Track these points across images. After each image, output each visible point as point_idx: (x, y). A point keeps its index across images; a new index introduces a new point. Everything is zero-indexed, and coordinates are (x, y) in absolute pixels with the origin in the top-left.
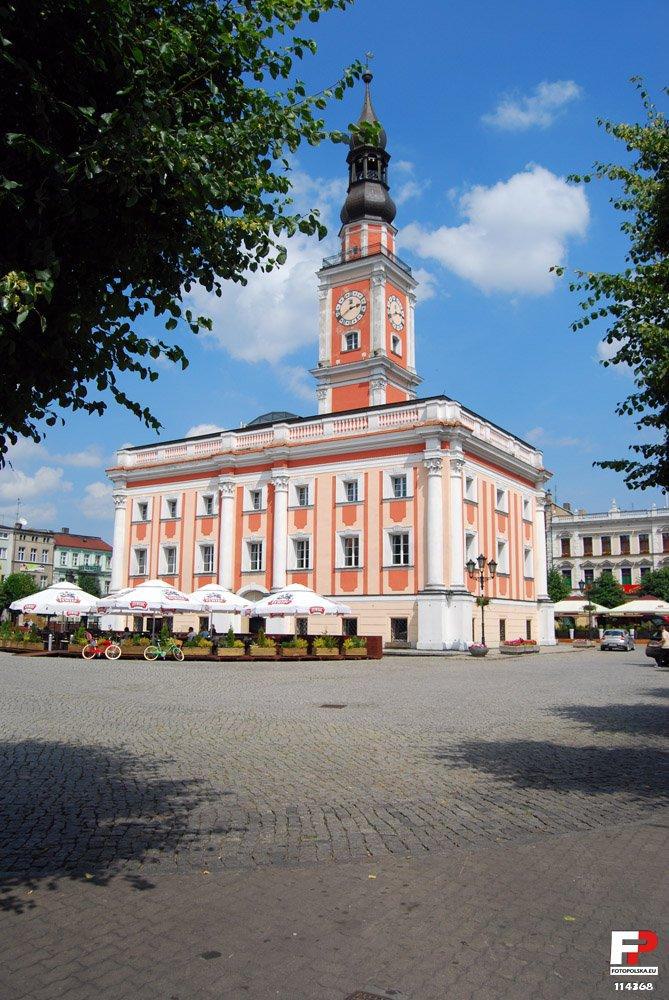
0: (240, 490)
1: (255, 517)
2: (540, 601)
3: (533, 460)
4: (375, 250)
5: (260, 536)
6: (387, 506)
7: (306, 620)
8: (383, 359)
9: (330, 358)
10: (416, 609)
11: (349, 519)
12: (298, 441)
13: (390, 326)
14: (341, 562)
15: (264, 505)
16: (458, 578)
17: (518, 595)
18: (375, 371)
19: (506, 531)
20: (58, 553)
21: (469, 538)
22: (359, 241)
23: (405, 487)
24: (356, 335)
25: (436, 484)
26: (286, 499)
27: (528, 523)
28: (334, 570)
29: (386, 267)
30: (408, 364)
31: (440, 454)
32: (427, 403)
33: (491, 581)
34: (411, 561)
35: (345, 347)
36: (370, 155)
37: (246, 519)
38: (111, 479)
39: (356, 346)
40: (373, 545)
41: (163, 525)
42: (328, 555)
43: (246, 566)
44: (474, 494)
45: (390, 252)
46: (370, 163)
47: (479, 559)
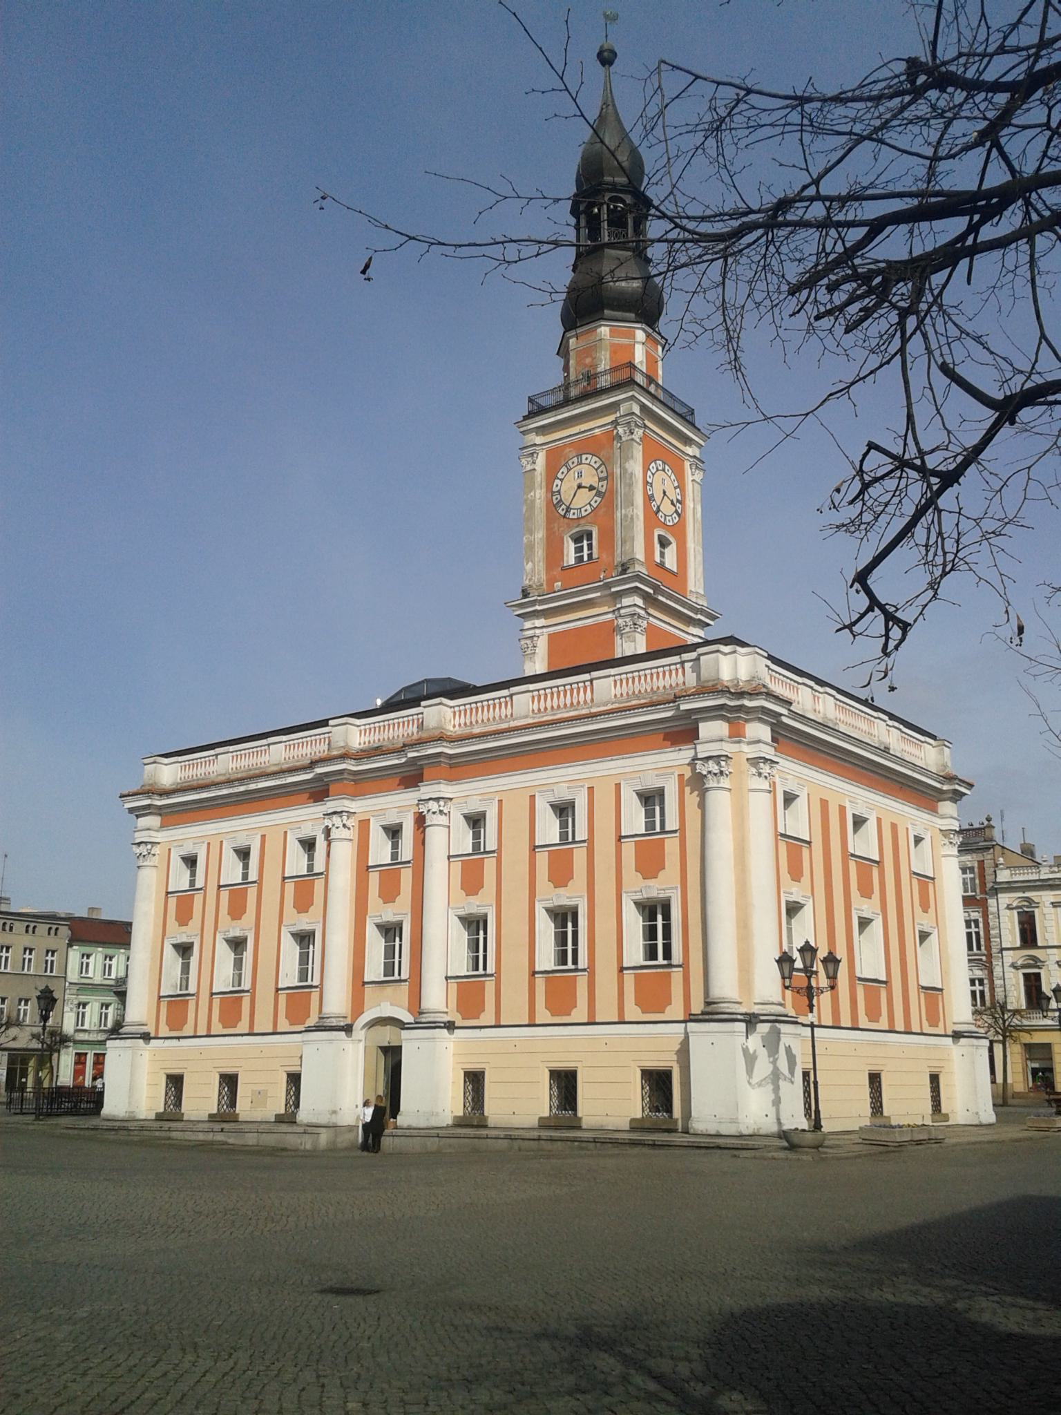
0: (364, 825)
1: (390, 876)
2: (957, 1036)
3: (927, 757)
4: (623, 375)
6: (629, 849)
8: (638, 578)
9: (544, 577)
10: (684, 1053)
11: (561, 874)
13: (652, 515)
14: (546, 958)
15: (407, 852)
16: (767, 988)
18: (626, 601)
20: (74, 955)
21: (793, 909)
24: (589, 536)
25: (720, 802)
26: (447, 839)
27: (925, 881)
28: (533, 973)
29: (643, 407)
30: (691, 586)
31: (728, 748)
32: (701, 650)
33: (826, 998)
34: (677, 957)
35: (570, 558)
36: (612, 199)
37: (374, 878)
38: (131, 810)
39: (590, 556)
40: (605, 925)
41: (225, 895)
43: (374, 969)
44: (799, 823)
45: (651, 380)
47: (801, 950)
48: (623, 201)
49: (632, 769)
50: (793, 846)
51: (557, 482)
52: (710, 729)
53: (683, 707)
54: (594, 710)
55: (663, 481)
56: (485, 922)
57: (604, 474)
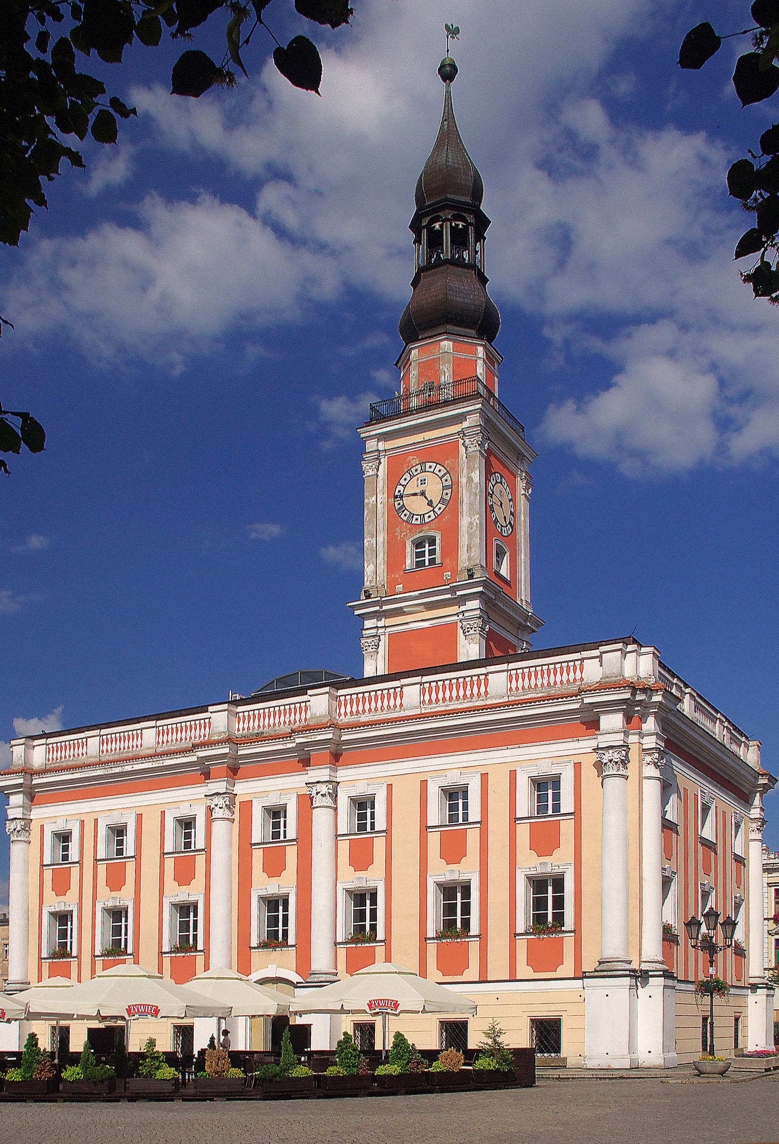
0: (247, 806)
5: (285, 884)
7: (122, 1029)
11: (453, 851)
12: (354, 719)
17: (686, 975)
19: (712, 874)
22: (437, 373)
23: (465, 806)
24: (432, 542)
27: (740, 861)
35: (409, 562)
36: (456, 218)
37: (258, 856)
39: (432, 561)
42: (407, 915)
46: (454, 229)
48: (464, 220)
49: (527, 757)
50: (667, 826)
51: (400, 488)
52: (612, 721)
53: (586, 701)
54: (489, 702)
55: (500, 490)
56: (127, 912)
57: (449, 483)
